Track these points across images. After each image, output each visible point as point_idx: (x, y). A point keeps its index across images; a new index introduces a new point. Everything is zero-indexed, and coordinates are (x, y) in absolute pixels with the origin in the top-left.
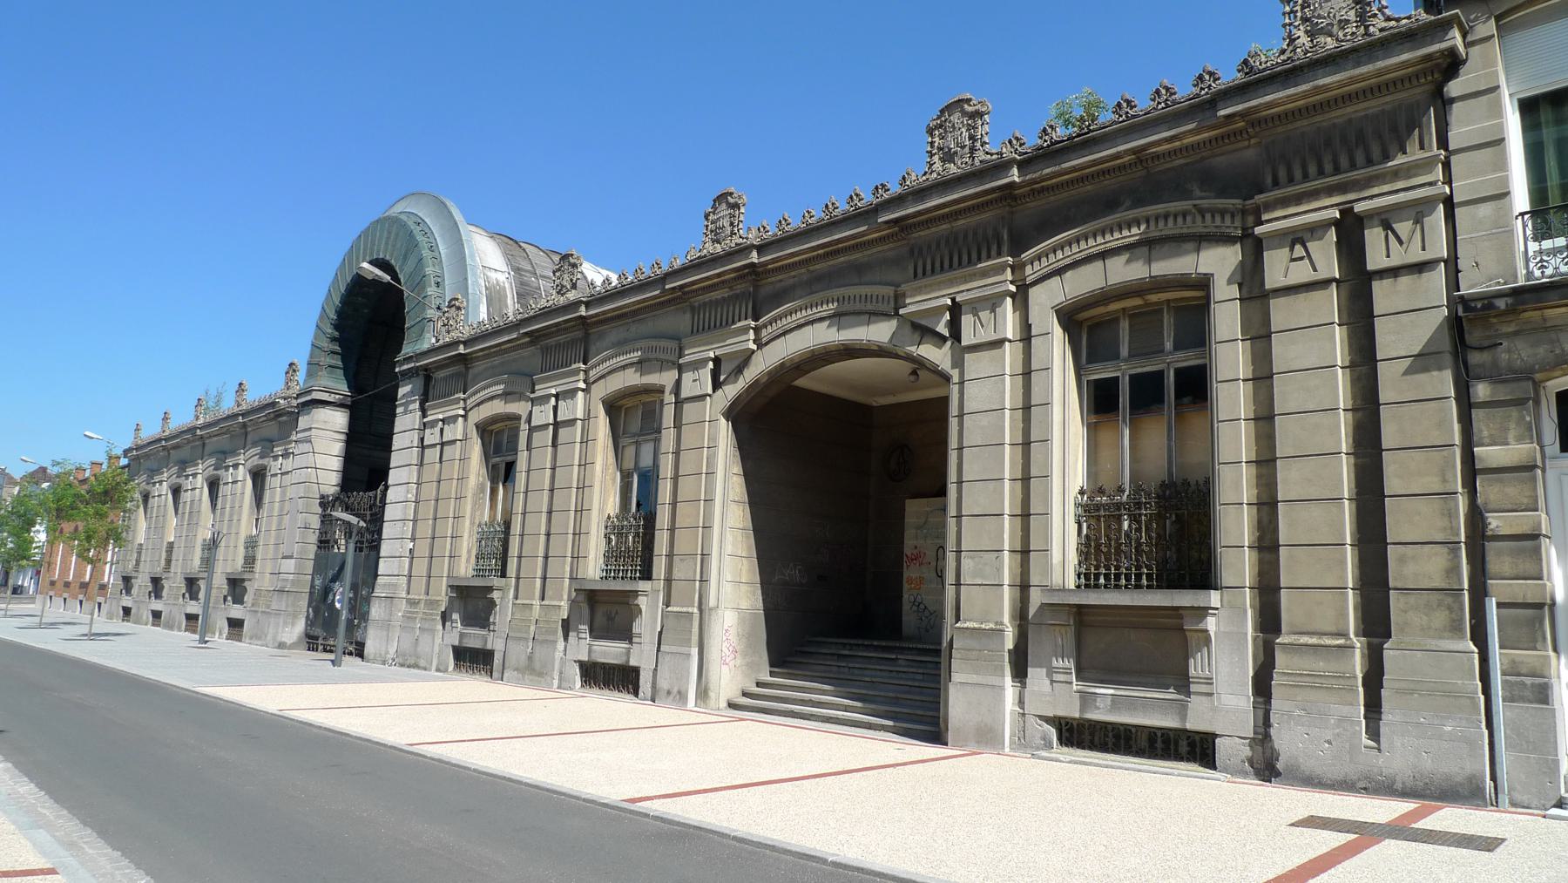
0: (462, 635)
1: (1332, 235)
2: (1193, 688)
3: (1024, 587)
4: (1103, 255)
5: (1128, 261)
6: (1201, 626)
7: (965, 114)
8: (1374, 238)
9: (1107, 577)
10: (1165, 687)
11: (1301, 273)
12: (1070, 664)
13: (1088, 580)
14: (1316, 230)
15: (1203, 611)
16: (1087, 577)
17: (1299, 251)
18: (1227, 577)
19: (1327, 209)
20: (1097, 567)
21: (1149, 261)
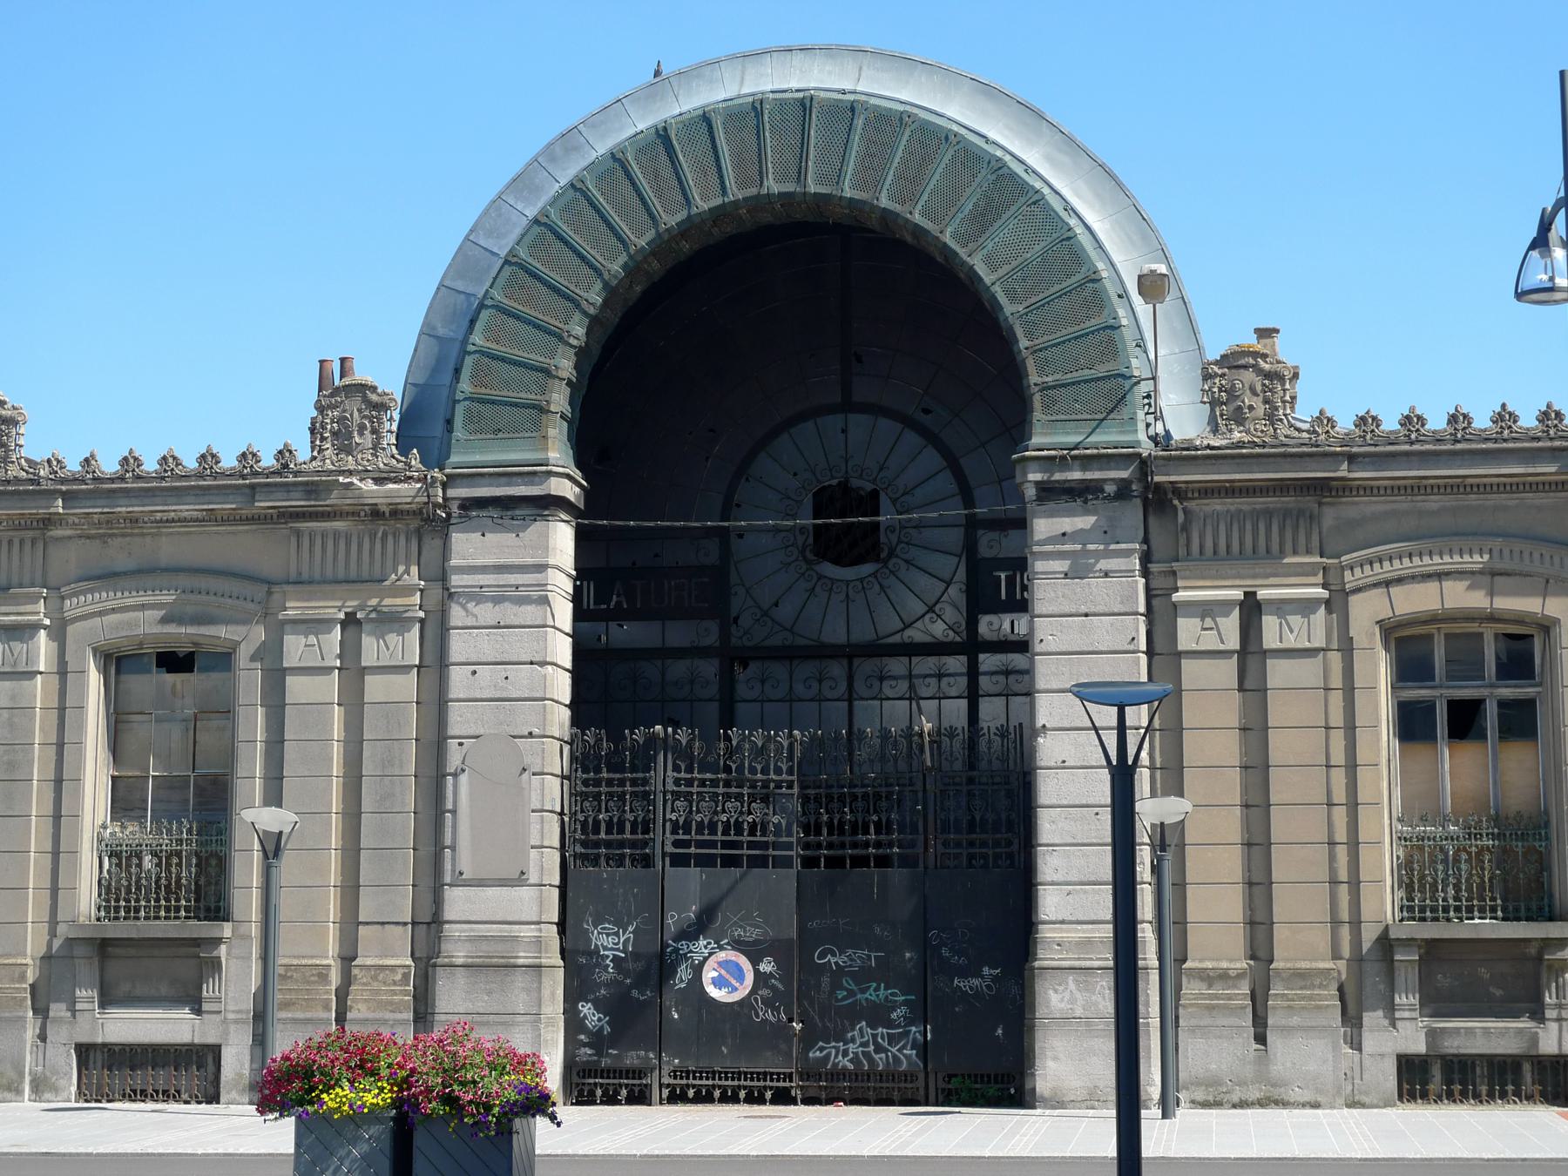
0: (1432, 1034)
1: (1236, 612)
2: (205, 1007)
3: (53, 922)
4: (1440, 576)
5: (1469, 588)
6: (215, 954)
7: (366, 400)
8: (1270, 623)
9: (168, 909)
10: (1515, 1015)
11: (1210, 642)
12: (1414, 1000)
13: (1409, 910)
14: (1223, 606)
15: (218, 941)
16: (107, 909)
17: (1209, 622)
18: (237, 911)
19: (334, 609)
20: (117, 900)
21: (1492, 594)
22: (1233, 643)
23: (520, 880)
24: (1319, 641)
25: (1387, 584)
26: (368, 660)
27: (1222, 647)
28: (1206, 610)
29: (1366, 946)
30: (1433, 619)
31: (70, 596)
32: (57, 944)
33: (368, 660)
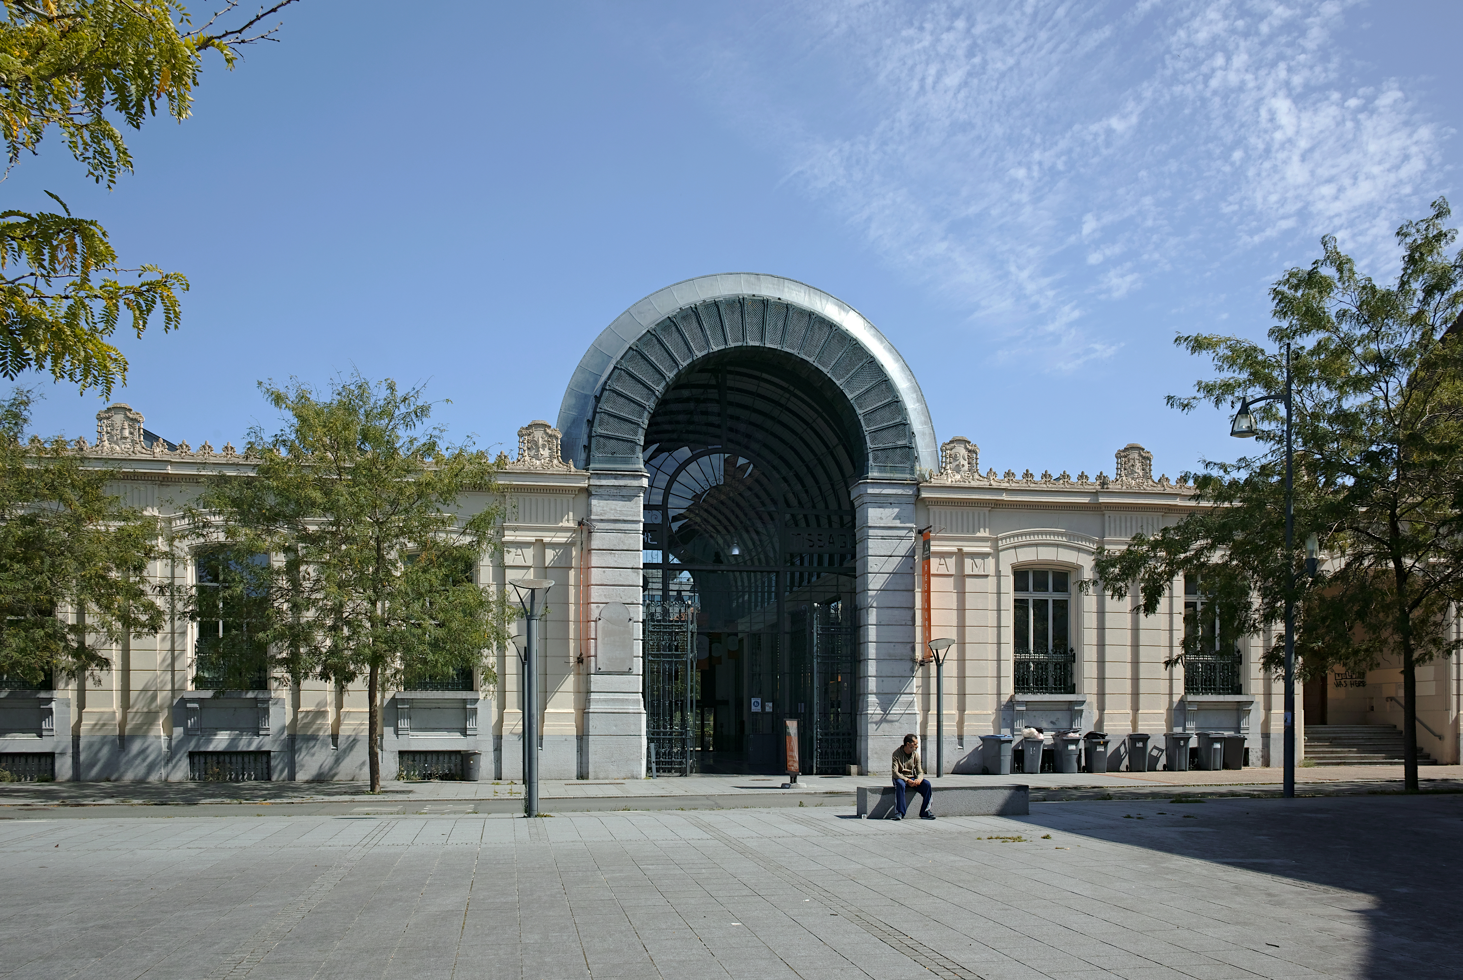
2: (468, 732)
4: (1037, 545)
7: (1140, 455)
8: (968, 562)
14: (950, 554)
15: (51, 700)
22: (952, 571)
23: (629, 672)
24: (530, 562)
25: (1015, 547)
26: (968, 571)
27: (524, 564)
28: (942, 555)
29: (1175, 705)
30: (1031, 563)
31: (1002, 539)
32: (175, 701)
33: (968, 571)
